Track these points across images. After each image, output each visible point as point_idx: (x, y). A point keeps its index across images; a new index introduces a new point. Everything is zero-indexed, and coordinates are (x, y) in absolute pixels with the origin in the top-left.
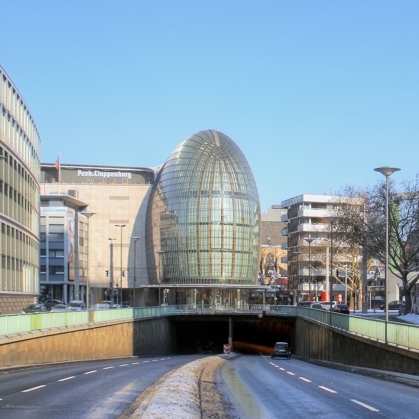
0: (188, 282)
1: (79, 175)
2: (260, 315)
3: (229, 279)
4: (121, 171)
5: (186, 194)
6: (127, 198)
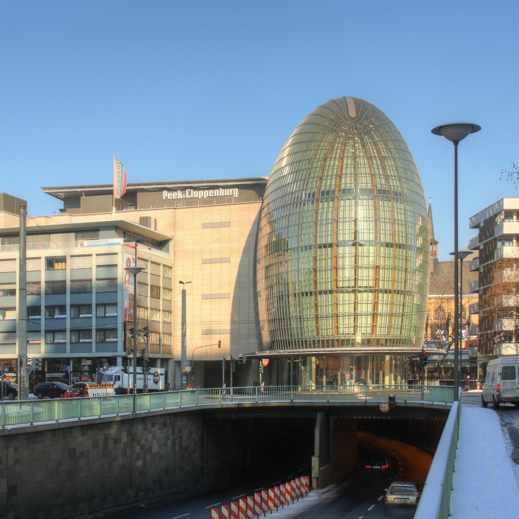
0: (312, 345)
1: (164, 198)
2: (384, 406)
3: (368, 338)
4: (224, 187)
5: (297, 200)
6: (227, 224)
